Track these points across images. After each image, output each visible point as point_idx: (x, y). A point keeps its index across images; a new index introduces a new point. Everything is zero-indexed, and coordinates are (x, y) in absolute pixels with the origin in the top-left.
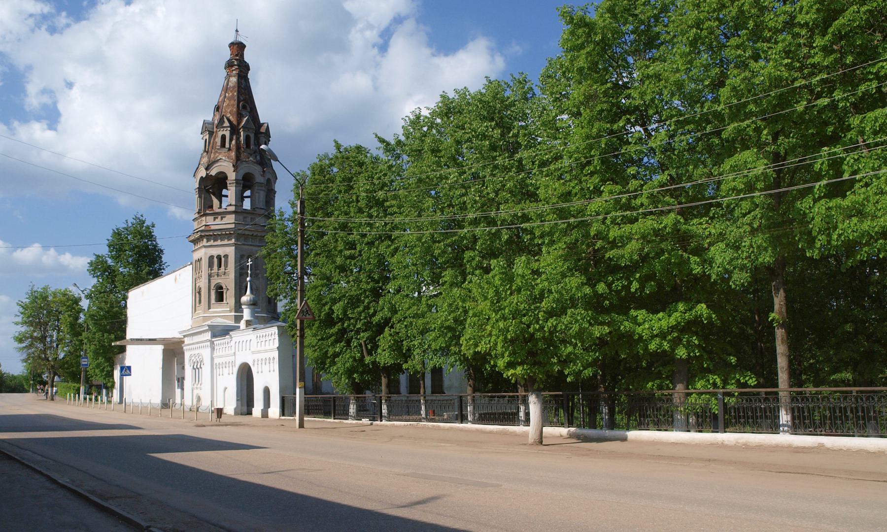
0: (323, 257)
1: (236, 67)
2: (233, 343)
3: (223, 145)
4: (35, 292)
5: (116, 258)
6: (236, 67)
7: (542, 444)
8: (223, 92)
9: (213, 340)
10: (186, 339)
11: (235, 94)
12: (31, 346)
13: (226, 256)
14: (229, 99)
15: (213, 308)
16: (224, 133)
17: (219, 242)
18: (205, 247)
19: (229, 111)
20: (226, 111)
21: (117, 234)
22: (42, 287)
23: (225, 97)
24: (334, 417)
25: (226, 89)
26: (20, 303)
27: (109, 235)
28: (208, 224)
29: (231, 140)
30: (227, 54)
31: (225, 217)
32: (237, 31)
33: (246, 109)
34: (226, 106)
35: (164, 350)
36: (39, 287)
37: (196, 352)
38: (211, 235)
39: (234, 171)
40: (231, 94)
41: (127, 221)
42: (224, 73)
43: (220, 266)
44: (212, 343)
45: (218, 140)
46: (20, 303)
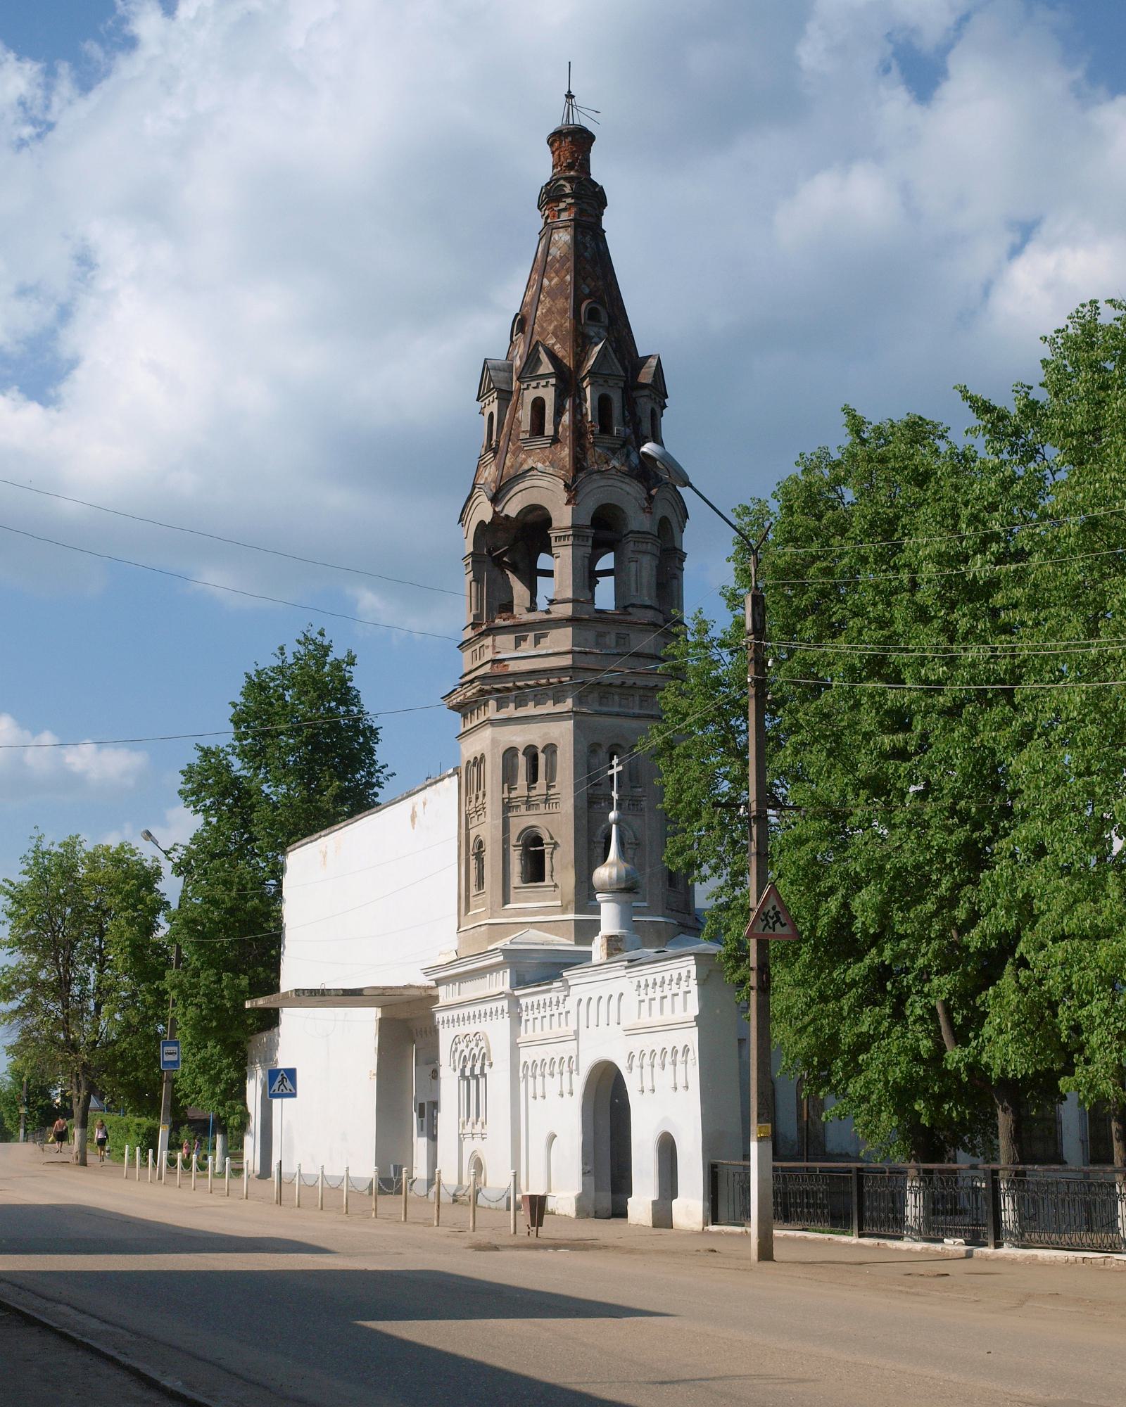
1: (570, 200)
5: (253, 755)
6: (570, 200)
9: (517, 993)
10: (446, 995)
11: (568, 278)
12: (32, 1006)
13: (551, 749)
14: (552, 294)
16: (541, 392)
17: (530, 710)
18: (492, 722)
19: (551, 328)
21: (257, 687)
23: (541, 288)
24: (860, 1229)
27: (234, 691)
28: (500, 657)
29: (559, 413)
31: (545, 636)
32: (570, 96)
34: (545, 315)
36: (53, 842)
37: (470, 1028)
38: (508, 690)
39: (568, 503)
40: (555, 280)
41: (282, 649)
43: (533, 777)
44: (515, 1002)
46: (7, 885)
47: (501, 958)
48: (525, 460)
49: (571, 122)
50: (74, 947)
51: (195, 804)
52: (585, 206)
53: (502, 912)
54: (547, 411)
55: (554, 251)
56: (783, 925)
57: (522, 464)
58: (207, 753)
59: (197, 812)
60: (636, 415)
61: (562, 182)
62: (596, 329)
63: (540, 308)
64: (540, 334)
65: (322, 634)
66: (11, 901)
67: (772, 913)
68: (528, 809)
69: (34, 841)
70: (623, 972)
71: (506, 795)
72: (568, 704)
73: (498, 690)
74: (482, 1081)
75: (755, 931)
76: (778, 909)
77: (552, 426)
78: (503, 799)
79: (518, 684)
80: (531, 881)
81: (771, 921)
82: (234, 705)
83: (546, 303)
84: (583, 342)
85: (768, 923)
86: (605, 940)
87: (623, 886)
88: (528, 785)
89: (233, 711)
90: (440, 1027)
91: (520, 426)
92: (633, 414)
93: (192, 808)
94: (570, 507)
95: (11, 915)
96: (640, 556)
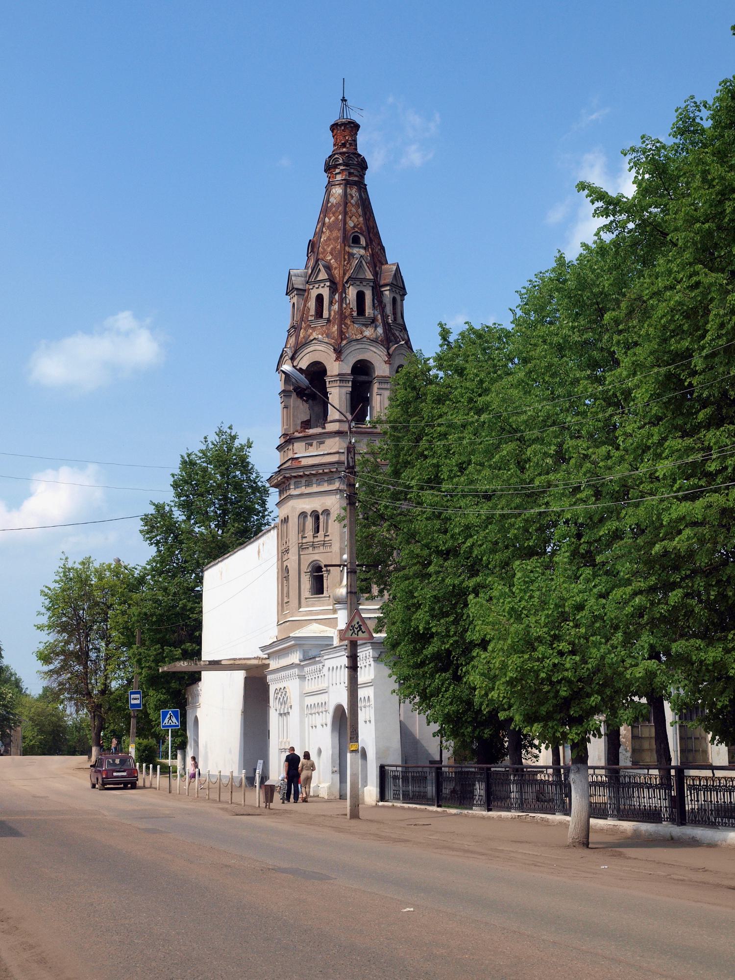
0: (649, 460)
1: (342, 167)
2: (325, 670)
3: (319, 314)
4: (69, 569)
5: (186, 506)
6: (342, 167)
7: (588, 847)
8: (322, 216)
10: (274, 664)
11: (340, 217)
12: (64, 668)
13: (327, 512)
14: (331, 227)
15: (308, 606)
17: (315, 489)
19: (329, 249)
20: (325, 250)
21: (188, 464)
22: (80, 560)
23: (324, 224)
24: (438, 802)
25: (326, 210)
26: (46, 590)
27: (175, 467)
28: (296, 456)
29: (331, 303)
30: (327, 145)
31: (323, 443)
32: (344, 100)
33: (359, 243)
34: (326, 241)
35: (246, 678)
36: (75, 562)
37: (281, 685)
38: (301, 476)
40: (333, 218)
41: (205, 438)
42: (324, 178)
43: (317, 530)
45: (312, 304)
46: (46, 590)
48: (311, 333)
49: (345, 117)
50: (91, 629)
51: (151, 539)
52: (352, 171)
53: (299, 614)
54: (325, 303)
55: (332, 200)
56: (363, 632)
57: (309, 336)
58: (159, 507)
59: (152, 544)
60: (382, 302)
61: (336, 156)
62: (357, 250)
63: (323, 236)
64: (323, 253)
65: (230, 428)
66: (49, 600)
67: (357, 626)
69: (63, 562)
71: (300, 542)
73: (295, 477)
75: (346, 636)
76: (360, 623)
77: (327, 312)
79: (306, 473)
80: (317, 594)
81: (356, 631)
82: (173, 475)
83: (326, 234)
84: (349, 258)
85: (354, 631)
89: (172, 479)
91: (309, 312)
92: (381, 302)
93: (148, 542)
95: (48, 609)
96: (382, 391)
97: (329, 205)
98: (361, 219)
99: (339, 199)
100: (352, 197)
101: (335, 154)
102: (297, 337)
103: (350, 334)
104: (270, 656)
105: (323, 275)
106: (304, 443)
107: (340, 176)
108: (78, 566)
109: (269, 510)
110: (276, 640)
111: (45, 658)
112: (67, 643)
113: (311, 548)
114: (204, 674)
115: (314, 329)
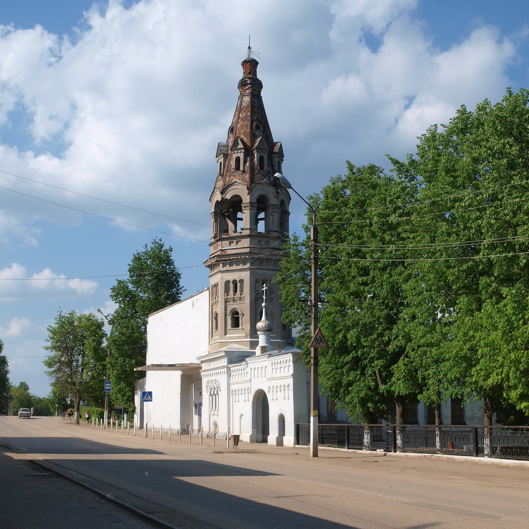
3: (237, 168)
5: (136, 283)
6: (249, 86)
8: (237, 113)
9: (229, 366)
10: (204, 366)
11: (249, 114)
12: (59, 370)
13: (242, 281)
14: (243, 119)
15: (230, 334)
16: (239, 155)
17: (234, 267)
18: (221, 272)
19: (242, 132)
20: (240, 132)
21: (137, 259)
24: (348, 446)
26: (50, 328)
27: (129, 260)
29: (245, 162)
30: (239, 74)
31: (240, 241)
32: (249, 48)
34: (240, 127)
36: (66, 313)
37: (213, 378)
38: (227, 260)
39: (248, 194)
40: (244, 114)
41: (146, 245)
43: (235, 291)
44: (229, 369)
45: (233, 163)
46: (50, 328)
47: (224, 354)
48: (233, 179)
49: (250, 57)
52: (255, 88)
56: (323, 343)
57: (232, 180)
58: (120, 282)
59: (116, 303)
61: (247, 79)
62: (258, 132)
64: (238, 134)
65: (160, 240)
67: (319, 339)
68: (233, 302)
69: (59, 313)
70: (267, 359)
71: (226, 297)
72: (248, 265)
73: (223, 260)
74: (217, 396)
76: (321, 337)
77: (243, 167)
78: (225, 298)
79: (230, 258)
82: (129, 265)
83: (241, 123)
86: (260, 348)
87: (267, 329)
88: (234, 294)
89: (129, 267)
90: (203, 377)
92: (272, 163)
93: (115, 301)
94: (249, 196)
95: (51, 338)
97: (242, 107)
98: (260, 116)
99: (247, 103)
100: (255, 103)
101: (245, 78)
102: (224, 181)
103: (256, 180)
104: (202, 362)
105: (241, 146)
106: (228, 241)
107: (248, 90)
108: (67, 315)
109: (181, 286)
110: (208, 354)
111: (50, 365)
112: (62, 356)
113: (232, 301)
114: (149, 373)
115: (234, 176)
